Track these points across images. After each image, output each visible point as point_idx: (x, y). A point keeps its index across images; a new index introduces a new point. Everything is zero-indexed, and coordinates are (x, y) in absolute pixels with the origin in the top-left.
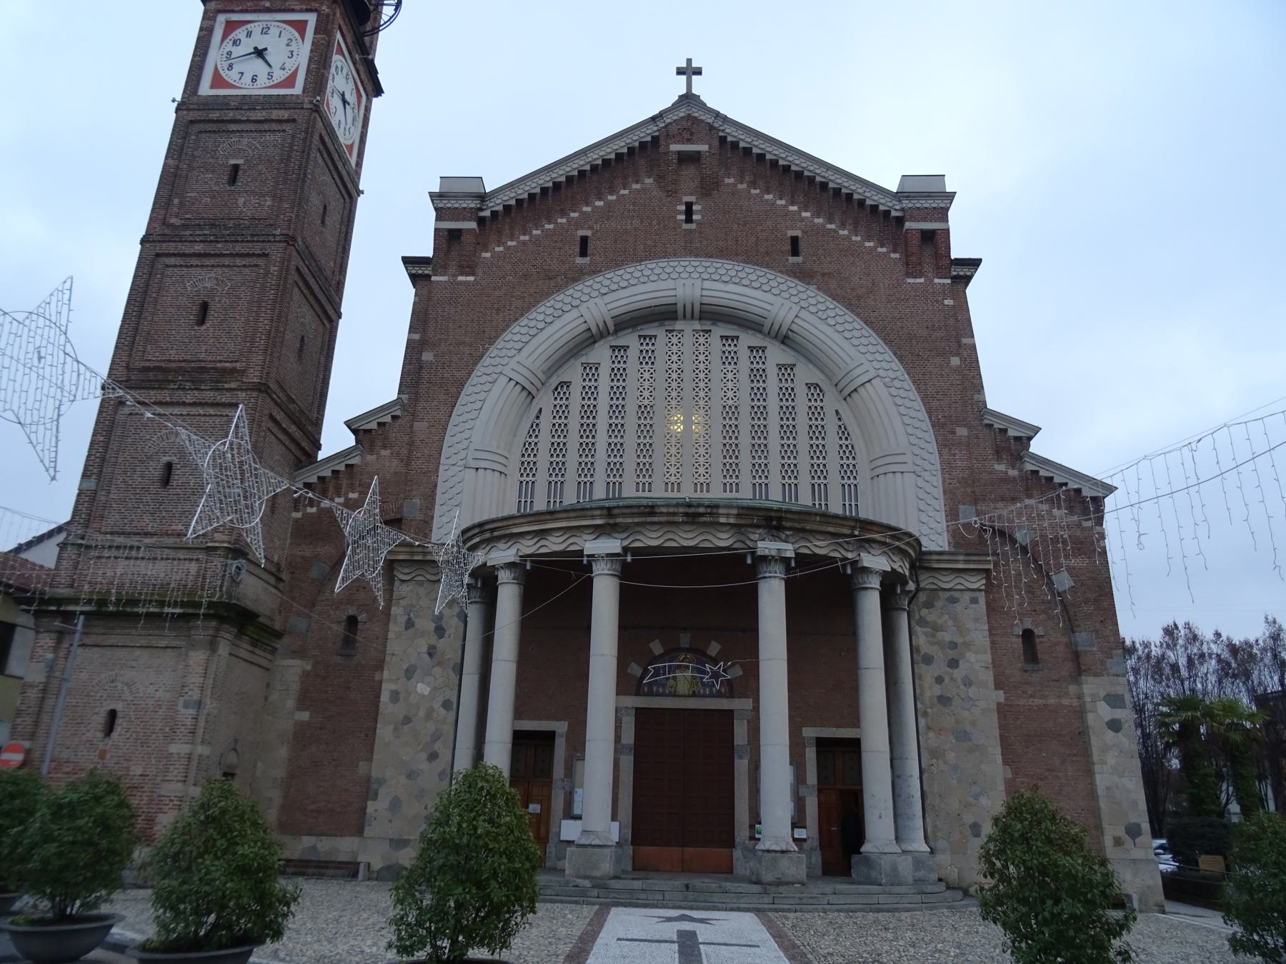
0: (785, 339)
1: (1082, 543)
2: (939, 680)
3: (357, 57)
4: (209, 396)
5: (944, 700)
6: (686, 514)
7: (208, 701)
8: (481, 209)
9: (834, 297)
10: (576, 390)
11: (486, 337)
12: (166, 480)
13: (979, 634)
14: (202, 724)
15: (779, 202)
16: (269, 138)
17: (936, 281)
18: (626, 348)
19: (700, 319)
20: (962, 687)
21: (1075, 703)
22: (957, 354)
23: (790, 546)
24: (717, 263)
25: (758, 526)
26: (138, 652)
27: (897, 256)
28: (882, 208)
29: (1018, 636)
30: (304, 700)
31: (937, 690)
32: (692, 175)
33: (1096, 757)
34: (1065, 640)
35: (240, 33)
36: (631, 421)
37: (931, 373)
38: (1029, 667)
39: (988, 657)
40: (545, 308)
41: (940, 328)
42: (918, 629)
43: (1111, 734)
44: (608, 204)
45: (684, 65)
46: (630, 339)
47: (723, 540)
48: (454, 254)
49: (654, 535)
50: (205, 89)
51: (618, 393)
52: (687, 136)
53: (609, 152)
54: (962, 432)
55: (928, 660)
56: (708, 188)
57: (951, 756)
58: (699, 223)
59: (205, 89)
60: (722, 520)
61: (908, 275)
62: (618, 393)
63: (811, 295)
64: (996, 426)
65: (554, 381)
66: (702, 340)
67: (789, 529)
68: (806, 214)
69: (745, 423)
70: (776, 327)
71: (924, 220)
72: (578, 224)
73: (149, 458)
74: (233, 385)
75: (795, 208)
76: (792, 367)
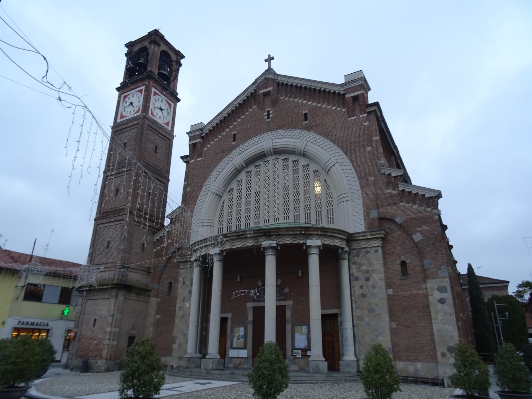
0: (304, 155)
1: (426, 219)
2: (361, 287)
3: (165, 93)
4: (117, 218)
5: (363, 295)
6: (237, 236)
7: (116, 314)
8: (202, 134)
9: (319, 134)
10: (235, 192)
11: (204, 178)
12: (108, 247)
13: (379, 265)
14: (114, 321)
15: (300, 101)
16: (134, 131)
17: (361, 116)
18: (251, 171)
19: (275, 154)
20: (371, 289)
21: (425, 292)
22: (371, 145)
23: (275, 242)
24: (277, 132)
25: (263, 236)
26: (101, 300)
27: (345, 110)
28: (337, 92)
29: (399, 264)
30: (158, 312)
31: (361, 291)
32: (273, 98)
33: (433, 316)
34: (420, 264)
35: (127, 99)
36: (253, 199)
37: (358, 156)
38: (403, 278)
39: (382, 275)
40: (222, 164)
41: (362, 136)
42: (353, 266)
43: (440, 305)
44: (242, 120)
45: (267, 58)
46: (252, 168)
47: (250, 243)
48: (196, 152)
49: (251, 241)
50: (119, 120)
51: (248, 189)
52: (265, 86)
53: (240, 101)
54: (372, 179)
55: (357, 279)
56: (275, 103)
57: (366, 319)
58: (272, 118)
59: (119, 120)
60: (249, 236)
61: (350, 117)
62: (248, 189)
63: (312, 135)
64: (386, 173)
65: (228, 189)
66: (276, 162)
67: (274, 235)
68: (310, 103)
69: (291, 192)
70: (299, 151)
71: (353, 92)
72: (232, 130)
73: (105, 240)
74: (122, 214)
75: (306, 102)
76: (308, 165)
